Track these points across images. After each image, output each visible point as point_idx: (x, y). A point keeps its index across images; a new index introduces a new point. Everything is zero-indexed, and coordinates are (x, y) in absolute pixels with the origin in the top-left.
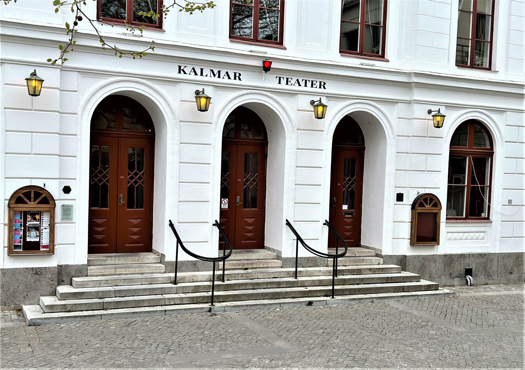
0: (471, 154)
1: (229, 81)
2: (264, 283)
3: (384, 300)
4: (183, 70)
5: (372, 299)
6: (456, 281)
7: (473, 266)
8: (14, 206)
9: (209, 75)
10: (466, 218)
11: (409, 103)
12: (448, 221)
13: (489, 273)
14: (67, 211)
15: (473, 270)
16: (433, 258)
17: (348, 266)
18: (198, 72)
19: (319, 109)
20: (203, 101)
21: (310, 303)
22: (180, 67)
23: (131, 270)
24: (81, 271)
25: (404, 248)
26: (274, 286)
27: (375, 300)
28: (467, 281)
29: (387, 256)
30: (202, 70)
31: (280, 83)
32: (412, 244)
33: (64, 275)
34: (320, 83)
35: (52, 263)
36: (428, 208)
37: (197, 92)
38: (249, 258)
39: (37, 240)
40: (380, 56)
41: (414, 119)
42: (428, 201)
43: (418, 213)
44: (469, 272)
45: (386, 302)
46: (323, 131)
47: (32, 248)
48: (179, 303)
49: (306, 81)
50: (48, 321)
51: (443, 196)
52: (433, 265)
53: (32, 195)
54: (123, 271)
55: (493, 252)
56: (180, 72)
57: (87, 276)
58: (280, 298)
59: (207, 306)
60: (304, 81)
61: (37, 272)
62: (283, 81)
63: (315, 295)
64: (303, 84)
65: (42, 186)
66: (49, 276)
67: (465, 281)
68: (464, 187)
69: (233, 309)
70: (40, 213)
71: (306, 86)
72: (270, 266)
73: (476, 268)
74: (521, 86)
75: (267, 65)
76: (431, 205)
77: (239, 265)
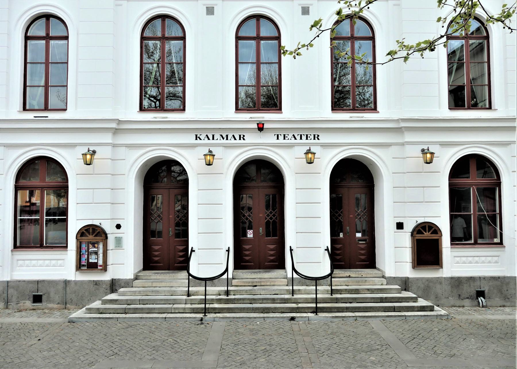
0: (475, 185)
1: (235, 142)
2: (260, 299)
3: (368, 319)
4: (199, 138)
5: (355, 318)
6: (467, 302)
7: (486, 289)
8: (80, 238)
9: (219, 139)
10: (476, 243)
11: (403, 144)
12: (453, 246)
13: (506, 296)
14: (119, 241)
15: (486, 292)
16: (439, 281)
17: (350, 285)
18: (211, 137)
19: (428, 157)
20: (429, 156)
21: (293, 319)
22: (196, 135)
23: (163, 284)
24: (128, 283)
25: (407, 270)
26: (269, 301)
27: (358, 319)
28: (479, 303)
29: (390, 277)
30: (213, 136)
31: (278, 139)
32: (414, 267)
33: (113, 286)
34: (314, 135)
35: (107, 277)
36: (427, 235)
37: (423, 150)
38: (262, 277)
39: (96, 261)
40: (372, 110)
41: (407, 157)
42: (427, 229)
43: (417, 240)
44: (481, 294)
45: (370, 320)
46: (320, 173)
47: (92, 266)
48: (182, 311)
49: (301, 135)
50: (80, 320)
51: (444, 223)
52: (438, 286)
53: (91, 231)
54: (158, 284)
55: (509, 276)
56: (196, 139)
57: (132, 287)
58: (269, 313)
59: (201, 315)
60: (299, 136)
61: (96, 283)
62: (281, 137)
63: (303, 311)
64: (298, 137)
65: (99, 224)
66: (104, 286)
67: (476, 303)
68: (471, 215)
69: (221, 320)
70: (98, 243)
71: (301, 139)
72: (276, 284)
73: (489, 290)
74: (513, 120)
75: (261, 126)
76: (430, 233)
77: (249, 282)
